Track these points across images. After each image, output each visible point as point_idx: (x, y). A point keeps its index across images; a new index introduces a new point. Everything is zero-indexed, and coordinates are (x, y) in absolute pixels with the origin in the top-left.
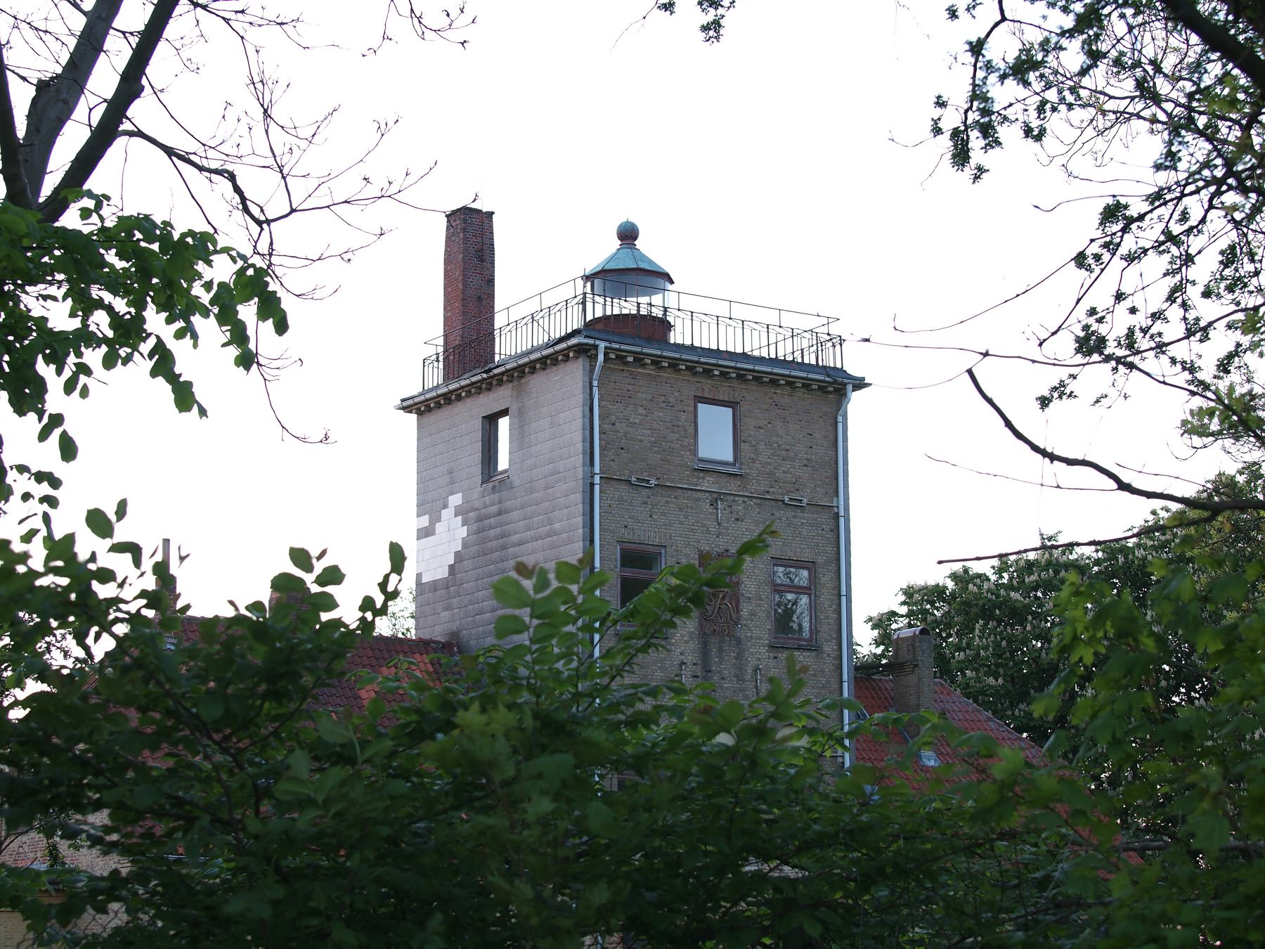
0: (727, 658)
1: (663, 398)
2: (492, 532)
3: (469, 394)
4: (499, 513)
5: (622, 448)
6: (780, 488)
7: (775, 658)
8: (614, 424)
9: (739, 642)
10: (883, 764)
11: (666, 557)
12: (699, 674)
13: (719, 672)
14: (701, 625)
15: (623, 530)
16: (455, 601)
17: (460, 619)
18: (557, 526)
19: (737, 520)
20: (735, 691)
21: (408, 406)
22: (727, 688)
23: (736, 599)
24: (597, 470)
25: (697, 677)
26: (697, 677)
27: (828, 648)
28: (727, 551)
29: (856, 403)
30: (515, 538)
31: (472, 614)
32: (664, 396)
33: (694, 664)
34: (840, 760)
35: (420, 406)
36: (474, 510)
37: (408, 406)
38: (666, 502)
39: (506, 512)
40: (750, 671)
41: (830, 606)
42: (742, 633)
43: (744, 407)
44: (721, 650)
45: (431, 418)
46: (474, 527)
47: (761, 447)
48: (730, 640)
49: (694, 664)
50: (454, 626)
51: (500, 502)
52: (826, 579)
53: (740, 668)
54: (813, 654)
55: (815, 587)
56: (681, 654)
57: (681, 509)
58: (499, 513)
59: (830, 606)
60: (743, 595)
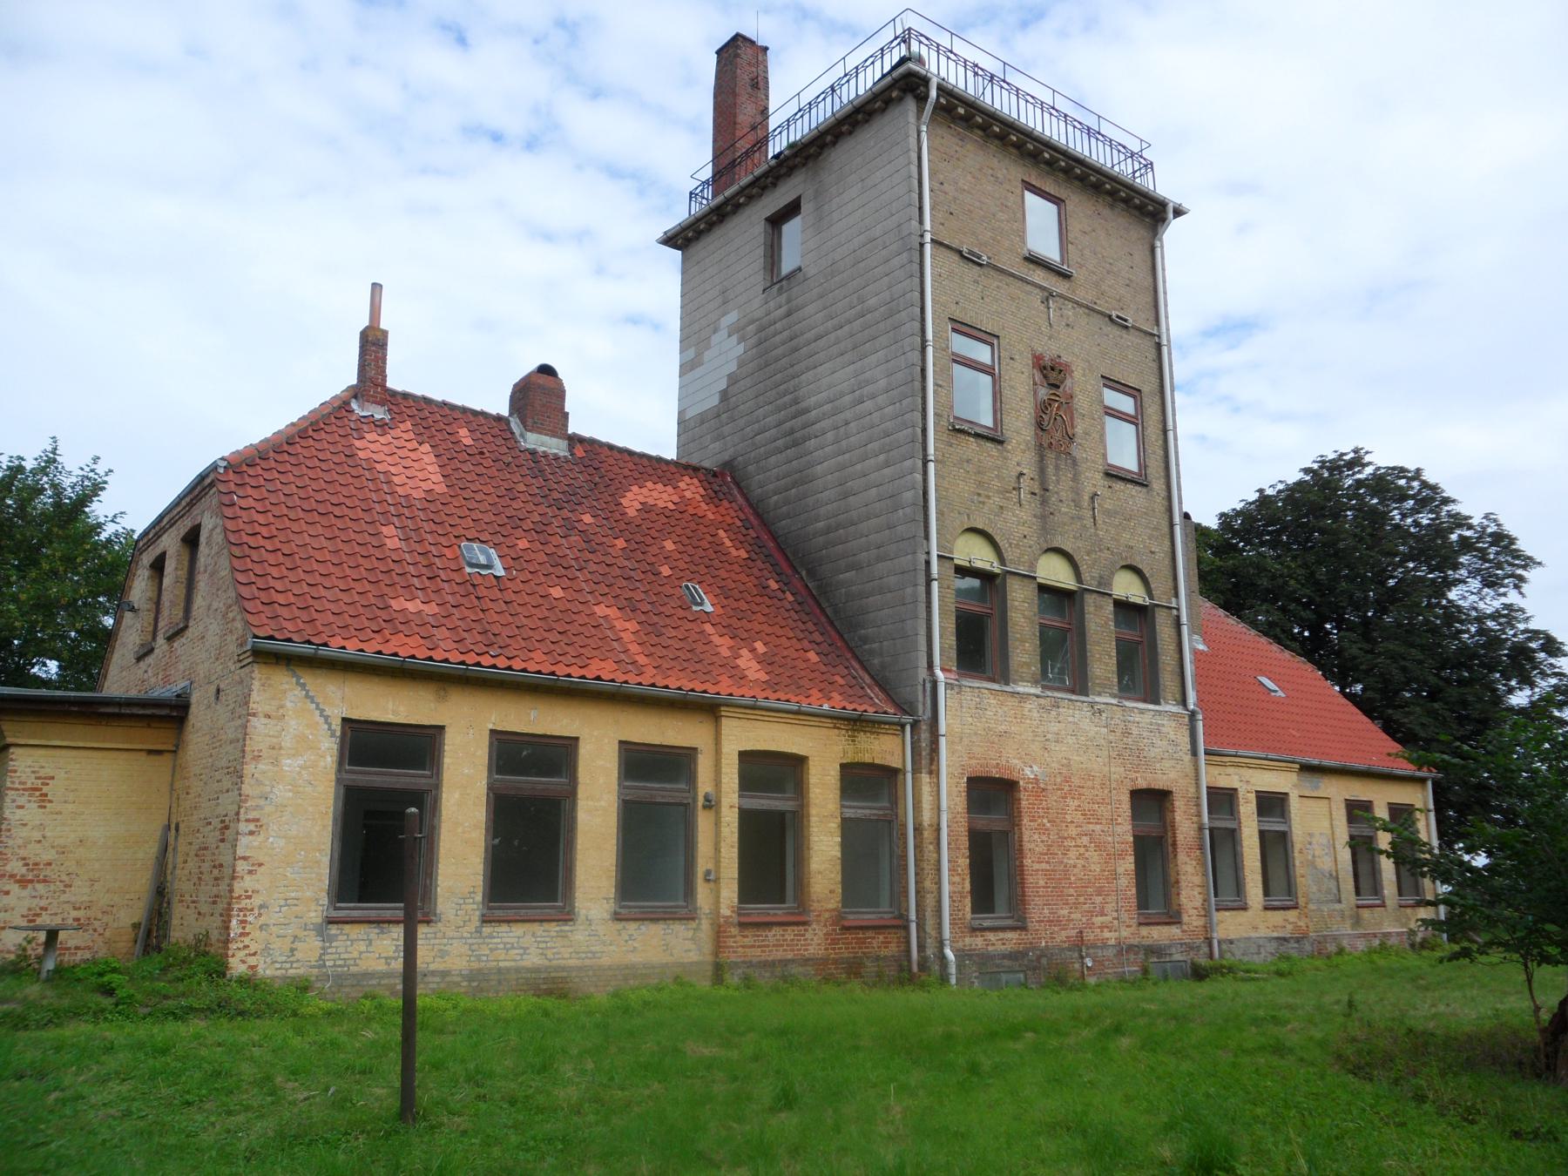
0: (1064, 478)
1: (990, 171)
2: (778, 339)
3: (750, 198)
4: (789, 314)
5: (951, 214)
6: (1107, 302)
7: (1110, 487)
8: (942, 184)
9: (1075, 462)
10: (1430, 516)
11: (999, 349)
12: (1037, 491)
13: (1056, 493)
14: (1036, 434)
15: (954, 307)
16: (727, 429)
17: (734, 446)
18: (872, 302)
19: (1068, 325)
20: (1072, 518)
21: (670, 240)
22: (1066, 513)
23: (1070, 411)
24: (928, 226)
25: (1035, 494)
26: (1035, 494)
27: (1158, 485)
28: (1059, 357)
29: (1174, 235)
30: (810, 335)
31: (751, 435)
32: (992, 169)
33: (1032, 479)
34: (1175, 612)
35: (680, 239)
36: (752, 322)
37: (670, 240)
38: (998, 287)
39: (798, 309)
40: (1086, 498)
41: (1156, 441)
42: (1076, 451)
43: (1070, 206)
44: (1057, 467)
45: (699, 249)
46: (753, 341)
47: (1087, 252)
48: (1066, 459)
49: (1032, 479)
50: (726, 456)
51: (789, 301)
52: (1152, 410)
53: (1077, 492)
54: (1144, 490)
55: (1142, 416)
56: (1018, 464)
57: (1013, 299)
58: (789, 314)
59: (1156, 441)
60: (1076, 409)
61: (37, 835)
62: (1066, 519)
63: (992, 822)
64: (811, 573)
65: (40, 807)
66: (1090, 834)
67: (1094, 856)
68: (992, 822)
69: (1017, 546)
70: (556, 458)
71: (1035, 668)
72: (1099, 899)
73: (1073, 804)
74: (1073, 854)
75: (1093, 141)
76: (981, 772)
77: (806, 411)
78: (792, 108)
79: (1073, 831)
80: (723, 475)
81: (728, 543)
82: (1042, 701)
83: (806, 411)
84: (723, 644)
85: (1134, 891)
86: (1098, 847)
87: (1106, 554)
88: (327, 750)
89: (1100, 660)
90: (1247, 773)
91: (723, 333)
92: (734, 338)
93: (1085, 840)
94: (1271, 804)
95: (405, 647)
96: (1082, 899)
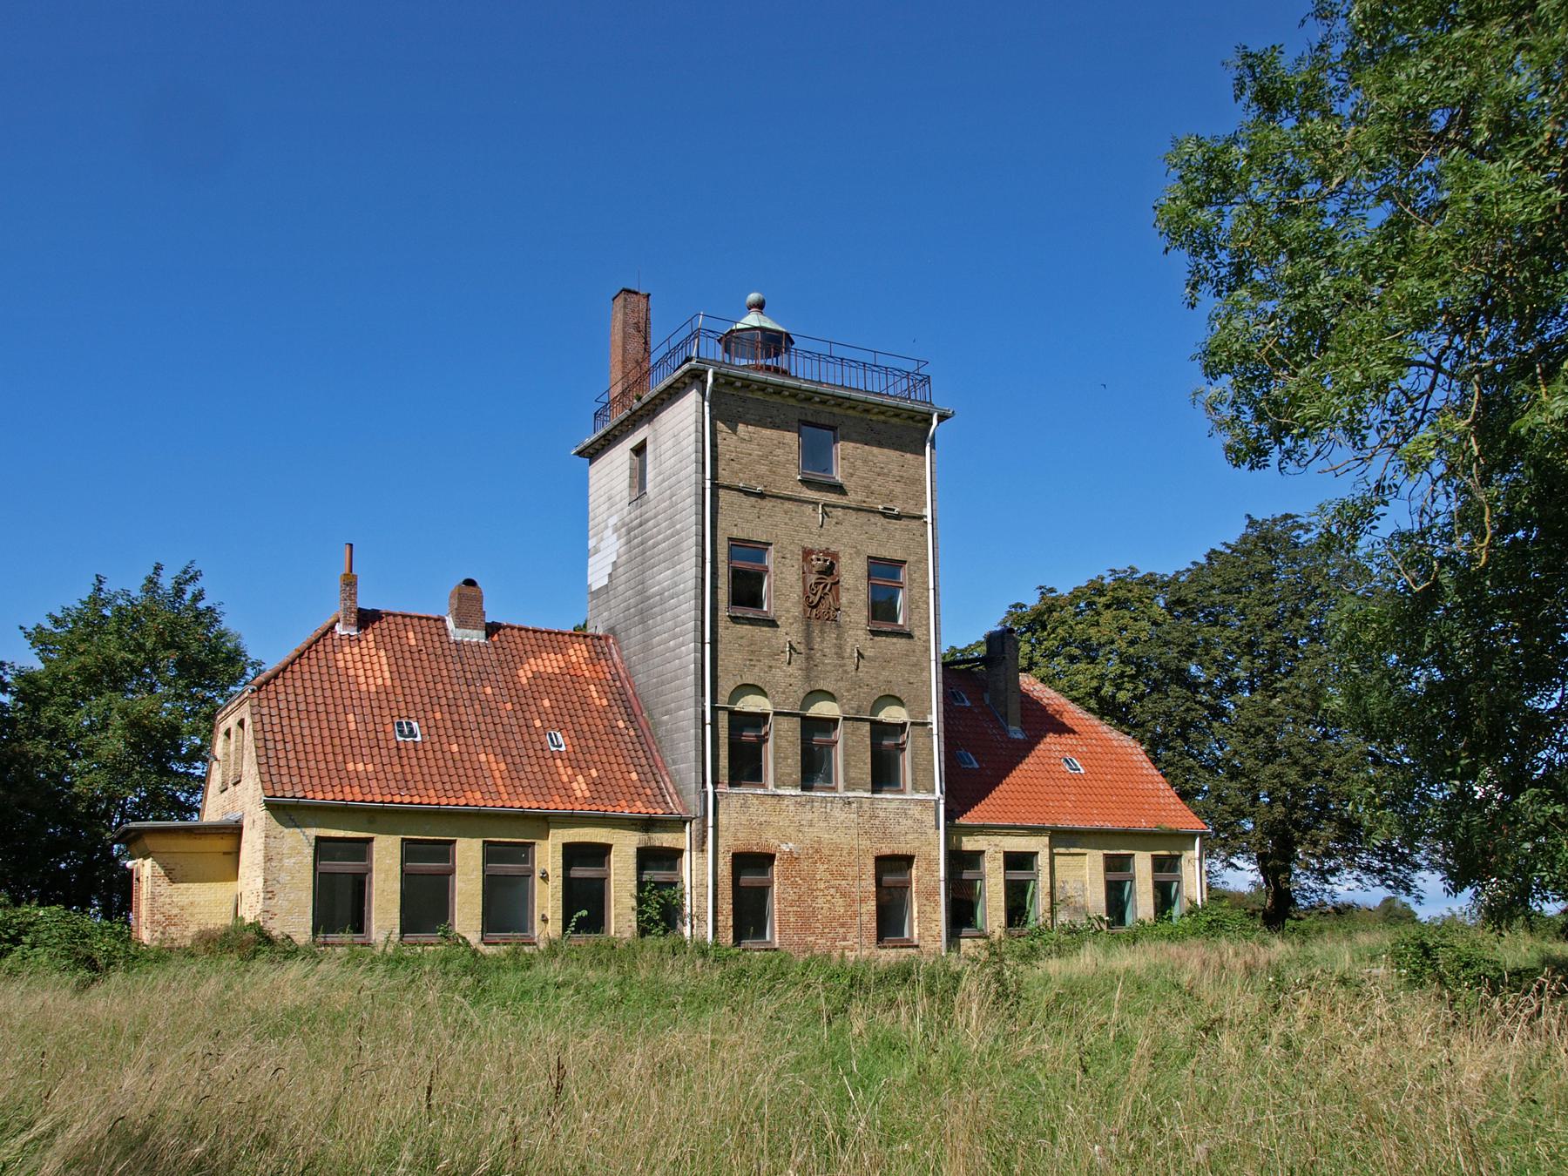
4: (641, 525)
9: (839, 626)
42: (842, 619)
44: (822, 631)
61: (168, 901)
62: (829, 668)
63: (1164, 876)
64: (650, 715)
65: (1421, 987)
66: (837, 888)
67: (839, 901)
68: (1164, 876)
69: (783, 693)
70: (478, 644)
71: (797, 776)
72: (841, 930)
73: (822, 868)
74: (820, 901)
75: (869, 373)
76: (742, 848)
77: (649, 598)
78: (664, 350)
79: (822, 885)
80: (607, 638)
81: (595, 694)
82: (799, 799)
83: (649, 598)
84: (565, 773)
85: (874, 924)
86: (843, 895)
87: (866, 689)
88: (309, 852)
89: (855, 766)
90: (997, 839)
91: (610, 531)
92: (615, 536)
93: (832, 891)
94: (1018, 861)
95: (353, 795)
96: (827, 930)
